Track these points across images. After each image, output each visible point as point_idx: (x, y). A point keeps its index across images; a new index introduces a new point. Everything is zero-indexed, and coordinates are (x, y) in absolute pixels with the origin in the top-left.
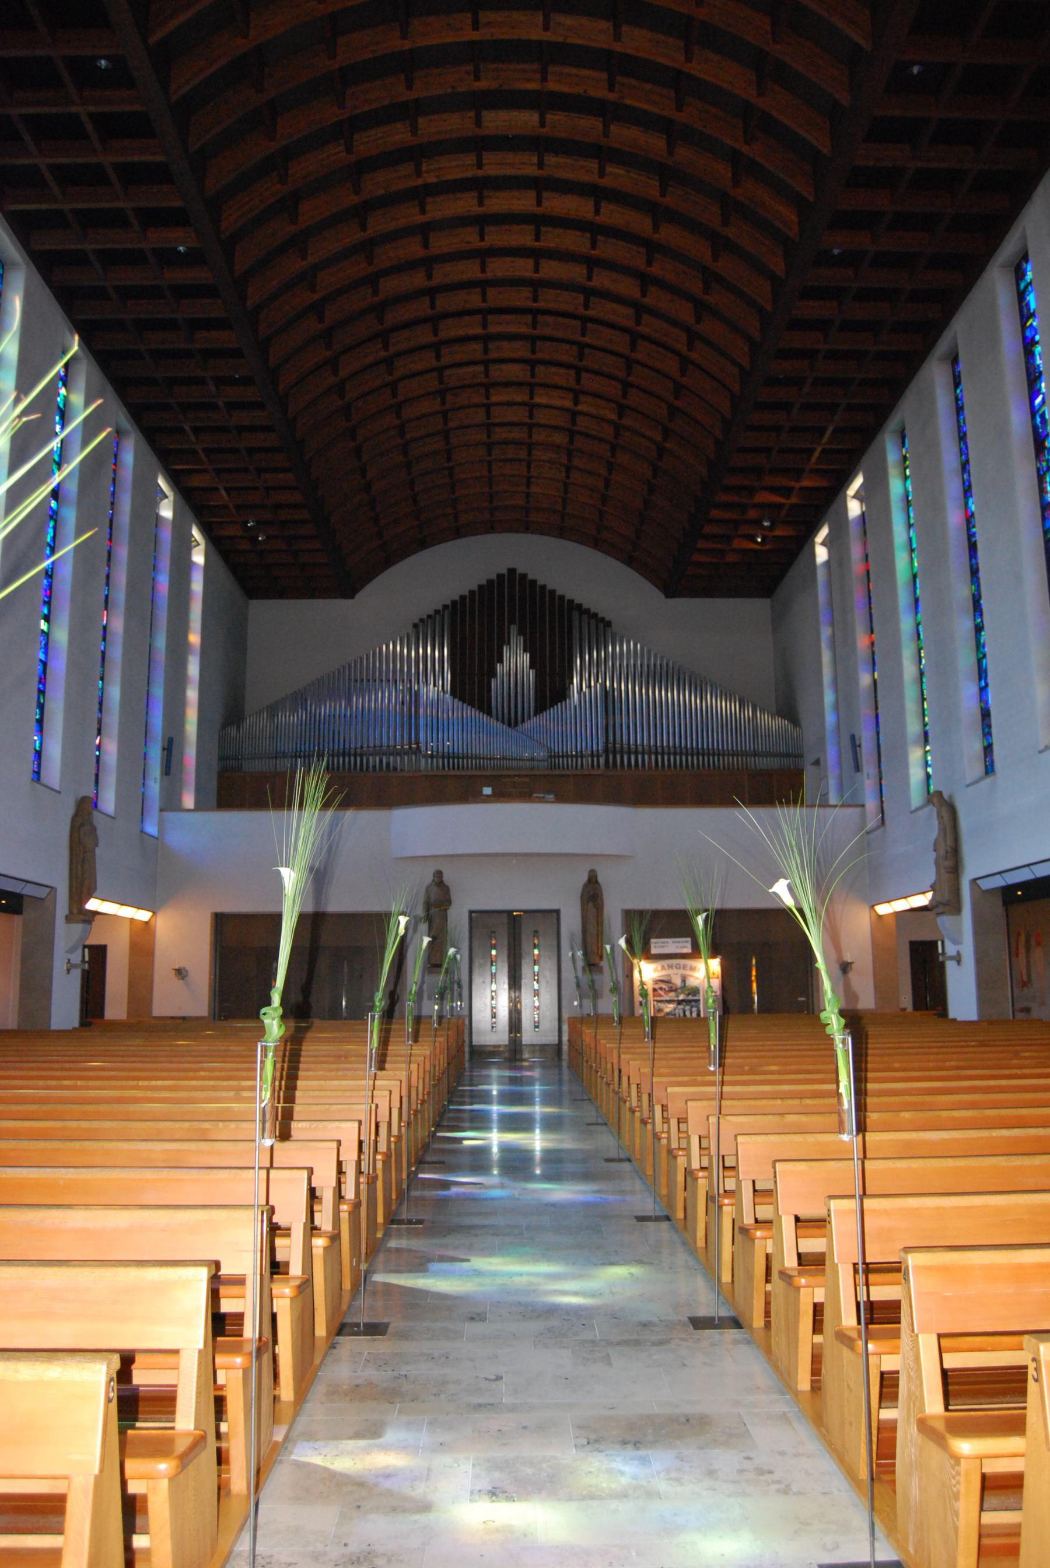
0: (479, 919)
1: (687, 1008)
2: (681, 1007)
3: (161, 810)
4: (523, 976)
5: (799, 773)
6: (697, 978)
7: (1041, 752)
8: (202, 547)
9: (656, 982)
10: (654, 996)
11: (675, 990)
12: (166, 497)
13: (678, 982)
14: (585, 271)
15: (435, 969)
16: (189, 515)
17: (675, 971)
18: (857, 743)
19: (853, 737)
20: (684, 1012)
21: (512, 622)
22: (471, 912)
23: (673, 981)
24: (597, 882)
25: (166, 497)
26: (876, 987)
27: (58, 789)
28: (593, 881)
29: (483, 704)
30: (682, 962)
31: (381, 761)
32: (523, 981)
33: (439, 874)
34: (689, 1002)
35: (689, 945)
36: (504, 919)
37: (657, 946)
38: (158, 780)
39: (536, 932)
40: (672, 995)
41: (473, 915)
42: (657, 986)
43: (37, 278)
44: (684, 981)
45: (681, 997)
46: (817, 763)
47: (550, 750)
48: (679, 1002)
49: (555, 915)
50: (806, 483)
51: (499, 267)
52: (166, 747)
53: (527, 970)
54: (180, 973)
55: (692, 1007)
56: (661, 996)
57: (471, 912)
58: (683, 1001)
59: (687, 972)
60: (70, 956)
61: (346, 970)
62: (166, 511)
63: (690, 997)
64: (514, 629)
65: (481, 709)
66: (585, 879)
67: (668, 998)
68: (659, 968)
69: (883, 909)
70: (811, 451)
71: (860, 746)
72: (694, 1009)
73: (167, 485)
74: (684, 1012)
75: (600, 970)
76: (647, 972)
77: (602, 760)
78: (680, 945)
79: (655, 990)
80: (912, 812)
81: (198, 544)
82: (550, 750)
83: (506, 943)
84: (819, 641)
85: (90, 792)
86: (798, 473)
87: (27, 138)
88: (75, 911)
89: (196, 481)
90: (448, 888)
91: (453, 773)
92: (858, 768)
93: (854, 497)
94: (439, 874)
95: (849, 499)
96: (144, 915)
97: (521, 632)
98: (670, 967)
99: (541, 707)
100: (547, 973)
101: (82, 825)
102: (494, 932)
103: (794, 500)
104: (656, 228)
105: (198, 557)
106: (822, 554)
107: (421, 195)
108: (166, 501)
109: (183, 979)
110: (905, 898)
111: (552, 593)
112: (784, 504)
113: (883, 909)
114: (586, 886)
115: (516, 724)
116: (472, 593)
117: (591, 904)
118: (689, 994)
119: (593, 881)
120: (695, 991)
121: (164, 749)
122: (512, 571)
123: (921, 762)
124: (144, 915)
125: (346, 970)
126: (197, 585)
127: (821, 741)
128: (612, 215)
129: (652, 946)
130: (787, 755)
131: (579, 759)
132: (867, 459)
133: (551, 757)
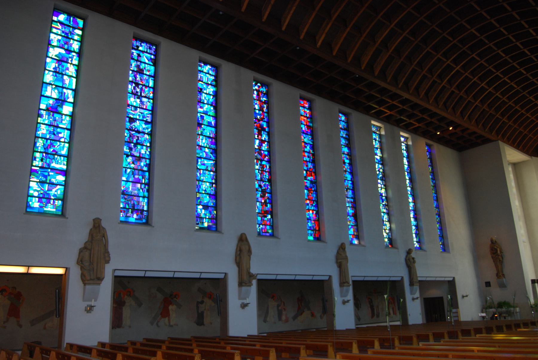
108: (382, 129)
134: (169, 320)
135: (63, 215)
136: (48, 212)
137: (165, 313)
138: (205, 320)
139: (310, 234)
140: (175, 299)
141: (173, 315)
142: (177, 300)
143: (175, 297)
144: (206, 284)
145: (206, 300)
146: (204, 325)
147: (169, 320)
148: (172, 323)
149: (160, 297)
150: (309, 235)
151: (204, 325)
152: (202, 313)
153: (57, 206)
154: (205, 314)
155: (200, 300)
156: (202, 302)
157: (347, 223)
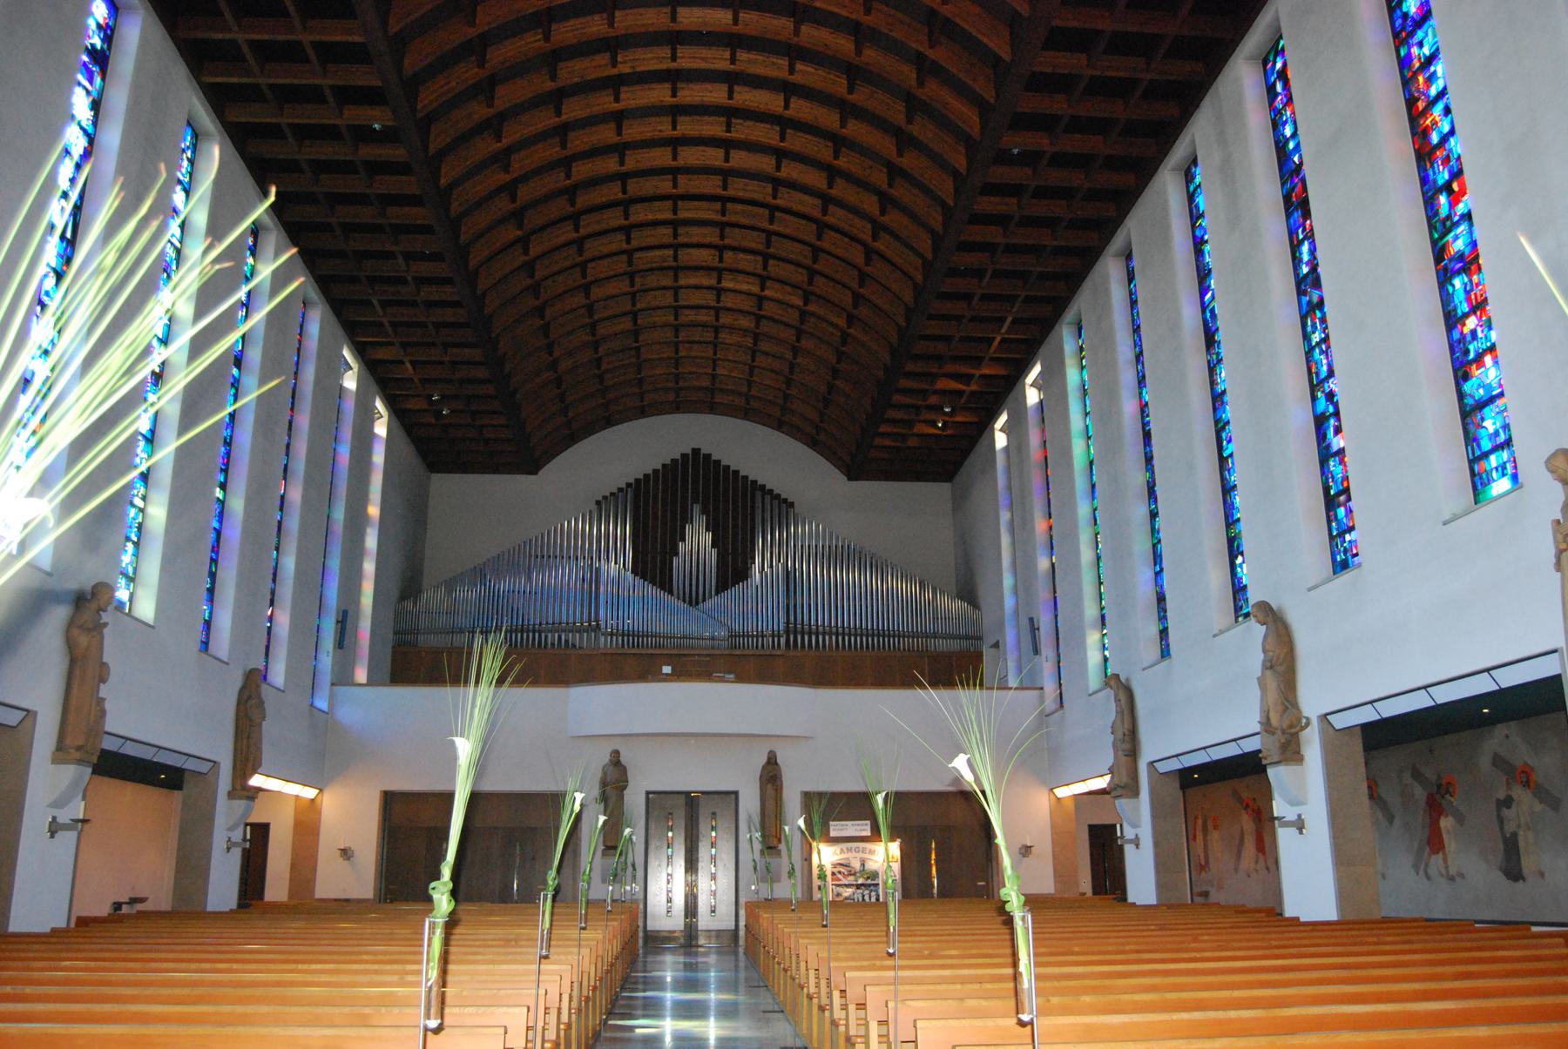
0: (657, 801)
1: (867, 892)
2: (859, 891)
3: (333, 684)
4: (700, 859)
5: (979, 656)
6: (876, 862)
7: (1090, 695)
8: (385, 419)
9: (835, 866)
10: (833, 880)
11: (854, 874)
12: (351, 369)
13: (857, 865)
14: (774, 162)
15: (611, 851)
16: (374, 387)
17: (854, 854)
18: (1036, 626)
19: (1031, 620)
20: (863, 896)
21: (695, 500)
22: (648, 793)
23: (852, 865)
24: (776, 763)
25: (351, 369)
26: (1055, 871)
27: (226, 660)
28: (772, 761)
29: (665, 584)
30: (861, 845)
31: (529, 578)
32: (700, 864)
33: (616, 753)
34: (870, 885)
35: (869, 828)
36: (682, 800)
37: (836, 829)
38: (331, 654)
39: (714, 814)
40: (851, 879)
41: (651, 796)
42: (835, 870)
43: (396, 424)
44: (863, 865)
45: (860, 881)
46: (996, 645)
47: (730, 630)
48: (858, 887)
49: (733, 796)
50: (986, 371)
51: (690, 156)
52: (340, 619)
53: (704, 852)
54: (346, 853)
55: (871, 891)
56: (840, 880)
57: (648, 793)
58: (862, 885)
59: (867, 856)
60: (56, 812)
61: (518, 852)
62: (350, 382)
63: (869, 882)
64: (697, 508)
65: (662, 588)
66: (764, 760)
67: (847, 883)
68: (838, 851)
69: (1062, 792)
70: (990, 341)
71: (1038, 629)
72: (873, 894)
73: (355, 358)
74: (863, 896)
75: (779, 853)
76: (827, 855)
77: (783, 640)
78: (859, 828)
79: (833, 874)
80: (1090, 695)
81: (382, 417)
82: (730, 630)
83: (683, 826)
84: (998, 524)
85: (261, 665)
86: (977, 361)
87: (228, 16)
88: (239, 787)
89: (381, 354)
90: (625, 768)
91: (633, 651)
92: (1036, 651)
93: (1001, 430)
94: (616, 753)
95: (1027, 387)
96: (309, 793)
97: (704, 511)
98: (849, 850)
99: (722, 586)
100: (724, 856)
101: (250, 697)
102: (671, 814)
103: (974, 387)
104: (836, 155)
105: (381, 429)
106: (1001, 440)
107: (616, 84)
109: (349, 859)
110: (1102, 776)
111: (736, 473)
112: (964, 391)
113: (1062, 792)
114: (764, 768)
115: (697, 603)
116: (655, 472)
117: (769, 786)
118: (868, 878)
119: (772, 761)
120: (874, 875)
121: (338, 622)
122: (696, 451)
123: (1099, 645)
124: (309, 793)
125: (518, 852)
126: (378, 457)
127: (1001, 625)
128: (801, 109)
129: (831, 828)
130: (967, 637)
131: (760, 639)
132: (1044, 350)
133: (732, 636)
134: (1445, 860)
135: (915, 1021)
136: (694, 832)
137: (1435, 843)
138: (1523, 862)
139: (1496, 468)
140: (1447, 796)
141: (1450, 844)
142: (1452, 799)
143: (1447, 792)
144: (1507, 736)
145: (1518, 792)
146: (1524, 879)
147: (1445, 860)
148: (1453, 871)
149: (1419, 793)
150: (1495, 475)
151: (1524, 879)
152: (1515, 835)
153: (568, 652)
154: (1522, 844)
155: (1502, 795)
156: (1508, 802)
157: (214, 493)
